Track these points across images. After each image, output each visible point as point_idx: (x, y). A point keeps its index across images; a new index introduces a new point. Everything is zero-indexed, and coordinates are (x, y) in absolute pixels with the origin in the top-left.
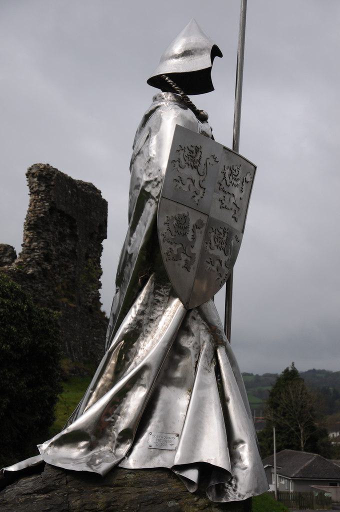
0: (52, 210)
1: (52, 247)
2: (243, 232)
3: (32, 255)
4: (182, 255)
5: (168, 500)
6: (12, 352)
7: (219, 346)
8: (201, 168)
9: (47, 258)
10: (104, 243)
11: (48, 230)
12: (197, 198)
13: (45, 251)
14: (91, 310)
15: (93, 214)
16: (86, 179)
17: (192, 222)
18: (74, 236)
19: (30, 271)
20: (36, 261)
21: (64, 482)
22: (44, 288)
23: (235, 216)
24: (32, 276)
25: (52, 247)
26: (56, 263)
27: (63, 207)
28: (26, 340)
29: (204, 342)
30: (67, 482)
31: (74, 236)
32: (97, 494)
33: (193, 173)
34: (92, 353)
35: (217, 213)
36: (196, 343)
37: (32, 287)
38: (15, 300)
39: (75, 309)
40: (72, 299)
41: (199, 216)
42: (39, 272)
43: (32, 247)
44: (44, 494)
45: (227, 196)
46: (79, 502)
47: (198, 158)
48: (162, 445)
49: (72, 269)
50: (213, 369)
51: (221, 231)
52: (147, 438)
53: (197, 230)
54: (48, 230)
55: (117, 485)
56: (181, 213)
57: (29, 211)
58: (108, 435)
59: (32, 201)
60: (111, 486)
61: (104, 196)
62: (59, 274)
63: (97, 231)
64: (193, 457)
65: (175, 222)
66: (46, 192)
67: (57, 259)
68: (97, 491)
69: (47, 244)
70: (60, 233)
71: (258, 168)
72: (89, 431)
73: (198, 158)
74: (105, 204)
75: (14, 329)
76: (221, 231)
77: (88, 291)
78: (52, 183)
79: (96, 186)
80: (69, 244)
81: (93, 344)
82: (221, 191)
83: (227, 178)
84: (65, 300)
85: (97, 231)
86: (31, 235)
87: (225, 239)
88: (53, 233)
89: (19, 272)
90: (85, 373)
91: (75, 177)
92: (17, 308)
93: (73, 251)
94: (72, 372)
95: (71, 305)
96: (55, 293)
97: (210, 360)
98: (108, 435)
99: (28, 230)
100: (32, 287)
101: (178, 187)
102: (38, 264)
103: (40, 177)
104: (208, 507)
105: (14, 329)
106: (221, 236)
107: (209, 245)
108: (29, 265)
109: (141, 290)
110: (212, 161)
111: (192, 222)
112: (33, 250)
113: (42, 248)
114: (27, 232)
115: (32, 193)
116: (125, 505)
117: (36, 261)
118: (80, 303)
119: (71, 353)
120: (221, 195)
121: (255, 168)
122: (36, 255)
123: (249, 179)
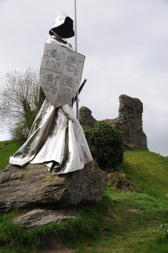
0: (125, 106)
1: (126, 116)
2: (81, 80)
3: (121, 118)
4: (51, 88)
5: (41, 174)
6: (108, 142)
7: (69, 120)
8: (57, 57)
9: (125, 118)
10: (142, 114)
11: (125, 111)
12: (56, 68)
13: (125, 117)
14: (139, 131)
15: (138, 106)
16: (136, 97)
17: (55, 77)
18: (133, 112)
19: (121, 122)
20: (122, 120)
21: (12, 168)
22: (125, 126)
23: (75, 74)
24: (121, 124)
25: (126, 116)
26: (128, 120)
27: (129, 105)
28: (112, 139)
29: (63, 119)
30: (13, 168)
31: (133, 112)
32: (20, 172)
33: (54, 59)
34: (140, 143)
35: (65, 72)
36: (60, 120)
37: (121, 126)
38: (108, 128)
39: (134, 131)
40: (133, 129)
41: (57, 74)
42: (123, 122)
43: (121, 116)
44: (5, 172)
45: (71, 67)
46: (14, 174)
47: (56, 53)
48: (44, 155)
49: (133, 121)
50: (65, 128)
51: (69, 79)
52: (40, 154)
53: (57, 79)
54: (125, 111)
55: (27, 169)
56: (50, 73)
57: (120, 107)
58: (29, 153)
59: (120, 104)
60: (25, 169)
61: (142, 101)
62: (129, 123)
63: (140, 111)
64: (55, 159)
65: (47, 77)
66: (124, 101)
67: (128, 119)
68: (20, 171)
69: (125, 115)
70: (129, 112)
71: (86, 58)
72: (22, 152)
73: (56, 53)
74: (142, 103)
75: (108, 136)
76: (69, 79)
77: (139, 127)
78: (125, 99)
79: (139, 99)
80: (131, 115)
81: (141, 140)
82: (68, 65)
83: (70, 60)
84: (131, 129)
85: (140, 111)
86: (120, 113)
87: (71, 82)
88: (127, 112)
89: (117, 122)
90: (138, 148)
91: (132, 97)
92: (109, 130)
93: (133, 116)
94: (134, 148)
95: (133, 130)
96: (128, 127)
97: (64, 125)
98: (29, 153)
99: (119, 112)
100: (121, 126)
101: (48, 64)
102: (123, 120)
103: (122, 98)
104: (54, 176)
105: (108, 136)
106: (69, 81)
107: (63, 84)
108: (120, 121)
109: (43, 103)
110: (62, 54)
111: (55, 77)
112: (121, 117)
113: (123, 116)
114: (119, 112)
115: (120, 102)
116: (27, 175)
117: (122, 120)
118: (136, 130)
119: (134, 143)
120: (68, 66)
121: (85, 57)
122: (122, 118)
123: (81, 60)
